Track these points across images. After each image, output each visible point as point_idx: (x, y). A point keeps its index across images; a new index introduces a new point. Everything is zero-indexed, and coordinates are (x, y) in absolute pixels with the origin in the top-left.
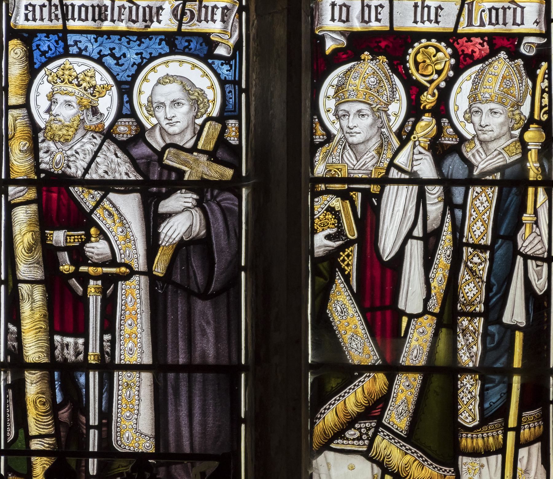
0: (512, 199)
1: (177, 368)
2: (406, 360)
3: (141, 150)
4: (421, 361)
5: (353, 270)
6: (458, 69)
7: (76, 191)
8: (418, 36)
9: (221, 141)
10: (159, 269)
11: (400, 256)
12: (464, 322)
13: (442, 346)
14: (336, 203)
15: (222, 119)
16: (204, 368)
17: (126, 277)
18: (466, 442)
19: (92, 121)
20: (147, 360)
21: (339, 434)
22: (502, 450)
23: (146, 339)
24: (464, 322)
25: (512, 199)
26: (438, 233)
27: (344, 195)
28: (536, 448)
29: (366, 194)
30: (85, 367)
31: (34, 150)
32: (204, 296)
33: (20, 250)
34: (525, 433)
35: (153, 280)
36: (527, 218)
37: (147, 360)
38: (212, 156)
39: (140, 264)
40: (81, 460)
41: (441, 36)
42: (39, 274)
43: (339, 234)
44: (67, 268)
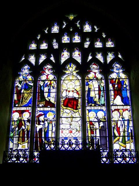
0: (129, 122)
1: (102, 137)
2: (121, 135)
3: (98, 119)
4: (121, 137)
5: (116, 128)
6: (123, 112)
7: (93, 122)
8: (120, 109)
9: (104, 118)
10: (100, 128)
11: (120, 127)
12: (125, 132)
13: (124, 134)
14: (114, 123)
15: (104, 116)
16: (104, 137)
17: (97, 129)
18: (126, 142)
19: (94, 117)
20: (99, 136)
21: (116, 142)
22: (129, 143)
23: (99, 134)
24: (125, 132)
25: (129, 122)
26: (123, 125)
27: (115, 122)
28: (132, 143)
29: (117, 122)
30: (94, 137)
31: (89, 119)
32: (104, 130)
33: (88, 127)
34: (131, 141)
35: (99, 129)
36: (130, 123)
37: (99, 136)
38: (104, 119)
39: (98, 128)
40: (54, 107)
41: (122, 109)
42: (90, 129)
43: (115, 125)
44: (92, 128)
